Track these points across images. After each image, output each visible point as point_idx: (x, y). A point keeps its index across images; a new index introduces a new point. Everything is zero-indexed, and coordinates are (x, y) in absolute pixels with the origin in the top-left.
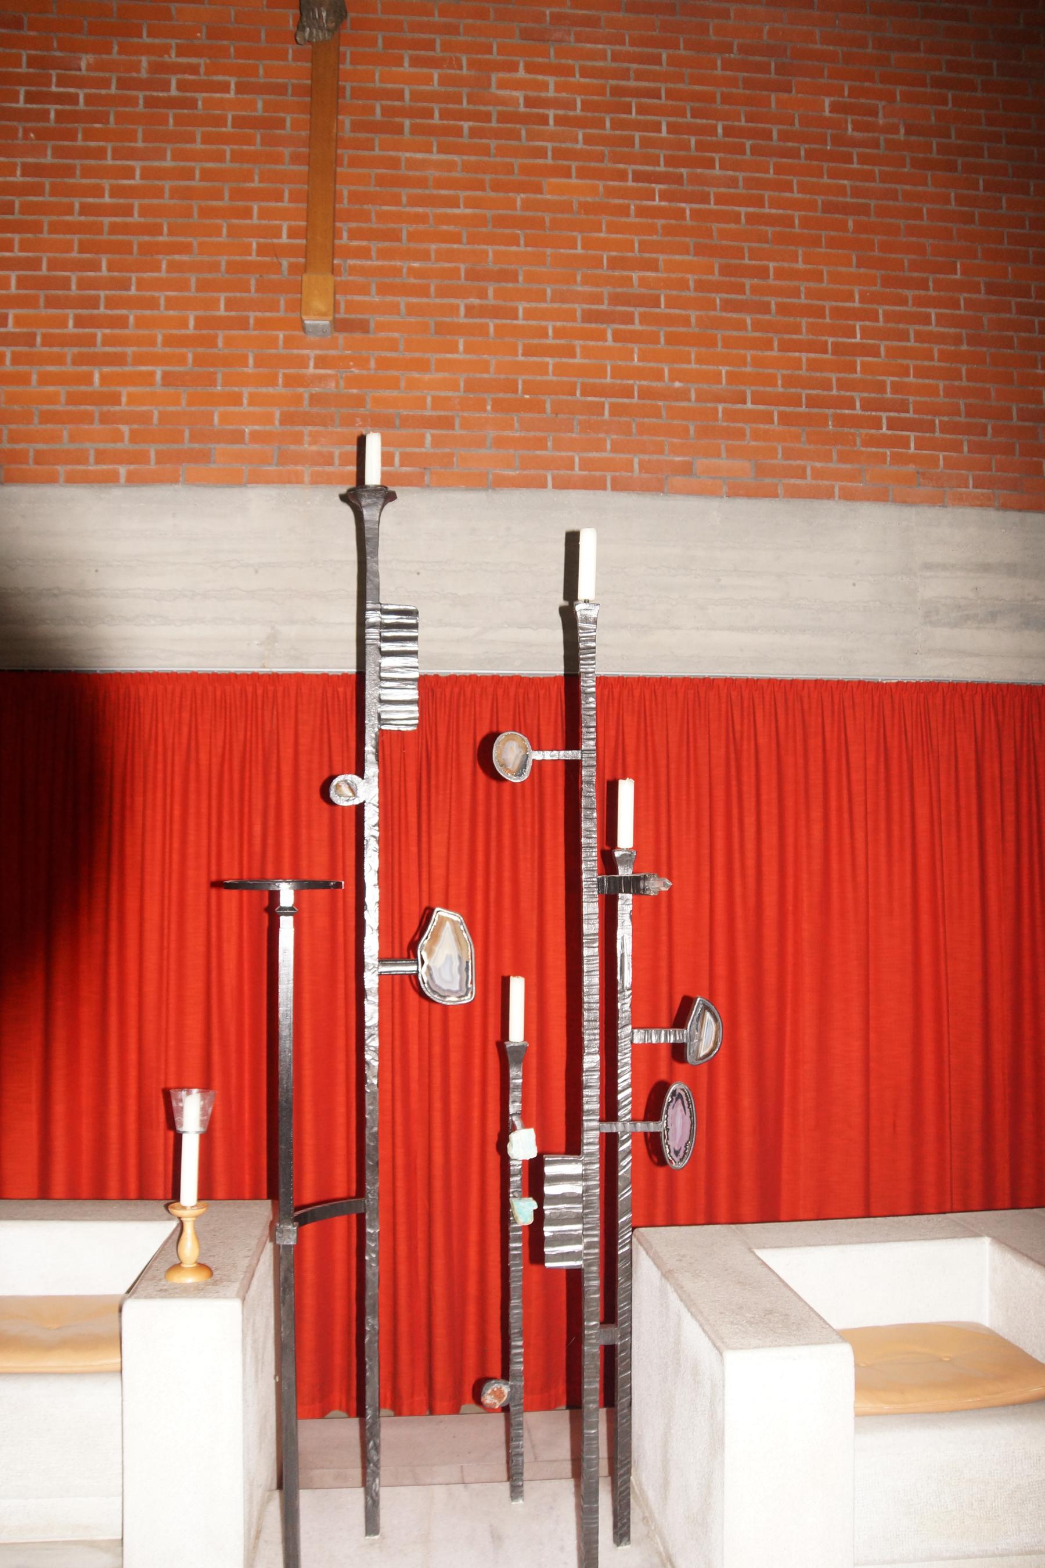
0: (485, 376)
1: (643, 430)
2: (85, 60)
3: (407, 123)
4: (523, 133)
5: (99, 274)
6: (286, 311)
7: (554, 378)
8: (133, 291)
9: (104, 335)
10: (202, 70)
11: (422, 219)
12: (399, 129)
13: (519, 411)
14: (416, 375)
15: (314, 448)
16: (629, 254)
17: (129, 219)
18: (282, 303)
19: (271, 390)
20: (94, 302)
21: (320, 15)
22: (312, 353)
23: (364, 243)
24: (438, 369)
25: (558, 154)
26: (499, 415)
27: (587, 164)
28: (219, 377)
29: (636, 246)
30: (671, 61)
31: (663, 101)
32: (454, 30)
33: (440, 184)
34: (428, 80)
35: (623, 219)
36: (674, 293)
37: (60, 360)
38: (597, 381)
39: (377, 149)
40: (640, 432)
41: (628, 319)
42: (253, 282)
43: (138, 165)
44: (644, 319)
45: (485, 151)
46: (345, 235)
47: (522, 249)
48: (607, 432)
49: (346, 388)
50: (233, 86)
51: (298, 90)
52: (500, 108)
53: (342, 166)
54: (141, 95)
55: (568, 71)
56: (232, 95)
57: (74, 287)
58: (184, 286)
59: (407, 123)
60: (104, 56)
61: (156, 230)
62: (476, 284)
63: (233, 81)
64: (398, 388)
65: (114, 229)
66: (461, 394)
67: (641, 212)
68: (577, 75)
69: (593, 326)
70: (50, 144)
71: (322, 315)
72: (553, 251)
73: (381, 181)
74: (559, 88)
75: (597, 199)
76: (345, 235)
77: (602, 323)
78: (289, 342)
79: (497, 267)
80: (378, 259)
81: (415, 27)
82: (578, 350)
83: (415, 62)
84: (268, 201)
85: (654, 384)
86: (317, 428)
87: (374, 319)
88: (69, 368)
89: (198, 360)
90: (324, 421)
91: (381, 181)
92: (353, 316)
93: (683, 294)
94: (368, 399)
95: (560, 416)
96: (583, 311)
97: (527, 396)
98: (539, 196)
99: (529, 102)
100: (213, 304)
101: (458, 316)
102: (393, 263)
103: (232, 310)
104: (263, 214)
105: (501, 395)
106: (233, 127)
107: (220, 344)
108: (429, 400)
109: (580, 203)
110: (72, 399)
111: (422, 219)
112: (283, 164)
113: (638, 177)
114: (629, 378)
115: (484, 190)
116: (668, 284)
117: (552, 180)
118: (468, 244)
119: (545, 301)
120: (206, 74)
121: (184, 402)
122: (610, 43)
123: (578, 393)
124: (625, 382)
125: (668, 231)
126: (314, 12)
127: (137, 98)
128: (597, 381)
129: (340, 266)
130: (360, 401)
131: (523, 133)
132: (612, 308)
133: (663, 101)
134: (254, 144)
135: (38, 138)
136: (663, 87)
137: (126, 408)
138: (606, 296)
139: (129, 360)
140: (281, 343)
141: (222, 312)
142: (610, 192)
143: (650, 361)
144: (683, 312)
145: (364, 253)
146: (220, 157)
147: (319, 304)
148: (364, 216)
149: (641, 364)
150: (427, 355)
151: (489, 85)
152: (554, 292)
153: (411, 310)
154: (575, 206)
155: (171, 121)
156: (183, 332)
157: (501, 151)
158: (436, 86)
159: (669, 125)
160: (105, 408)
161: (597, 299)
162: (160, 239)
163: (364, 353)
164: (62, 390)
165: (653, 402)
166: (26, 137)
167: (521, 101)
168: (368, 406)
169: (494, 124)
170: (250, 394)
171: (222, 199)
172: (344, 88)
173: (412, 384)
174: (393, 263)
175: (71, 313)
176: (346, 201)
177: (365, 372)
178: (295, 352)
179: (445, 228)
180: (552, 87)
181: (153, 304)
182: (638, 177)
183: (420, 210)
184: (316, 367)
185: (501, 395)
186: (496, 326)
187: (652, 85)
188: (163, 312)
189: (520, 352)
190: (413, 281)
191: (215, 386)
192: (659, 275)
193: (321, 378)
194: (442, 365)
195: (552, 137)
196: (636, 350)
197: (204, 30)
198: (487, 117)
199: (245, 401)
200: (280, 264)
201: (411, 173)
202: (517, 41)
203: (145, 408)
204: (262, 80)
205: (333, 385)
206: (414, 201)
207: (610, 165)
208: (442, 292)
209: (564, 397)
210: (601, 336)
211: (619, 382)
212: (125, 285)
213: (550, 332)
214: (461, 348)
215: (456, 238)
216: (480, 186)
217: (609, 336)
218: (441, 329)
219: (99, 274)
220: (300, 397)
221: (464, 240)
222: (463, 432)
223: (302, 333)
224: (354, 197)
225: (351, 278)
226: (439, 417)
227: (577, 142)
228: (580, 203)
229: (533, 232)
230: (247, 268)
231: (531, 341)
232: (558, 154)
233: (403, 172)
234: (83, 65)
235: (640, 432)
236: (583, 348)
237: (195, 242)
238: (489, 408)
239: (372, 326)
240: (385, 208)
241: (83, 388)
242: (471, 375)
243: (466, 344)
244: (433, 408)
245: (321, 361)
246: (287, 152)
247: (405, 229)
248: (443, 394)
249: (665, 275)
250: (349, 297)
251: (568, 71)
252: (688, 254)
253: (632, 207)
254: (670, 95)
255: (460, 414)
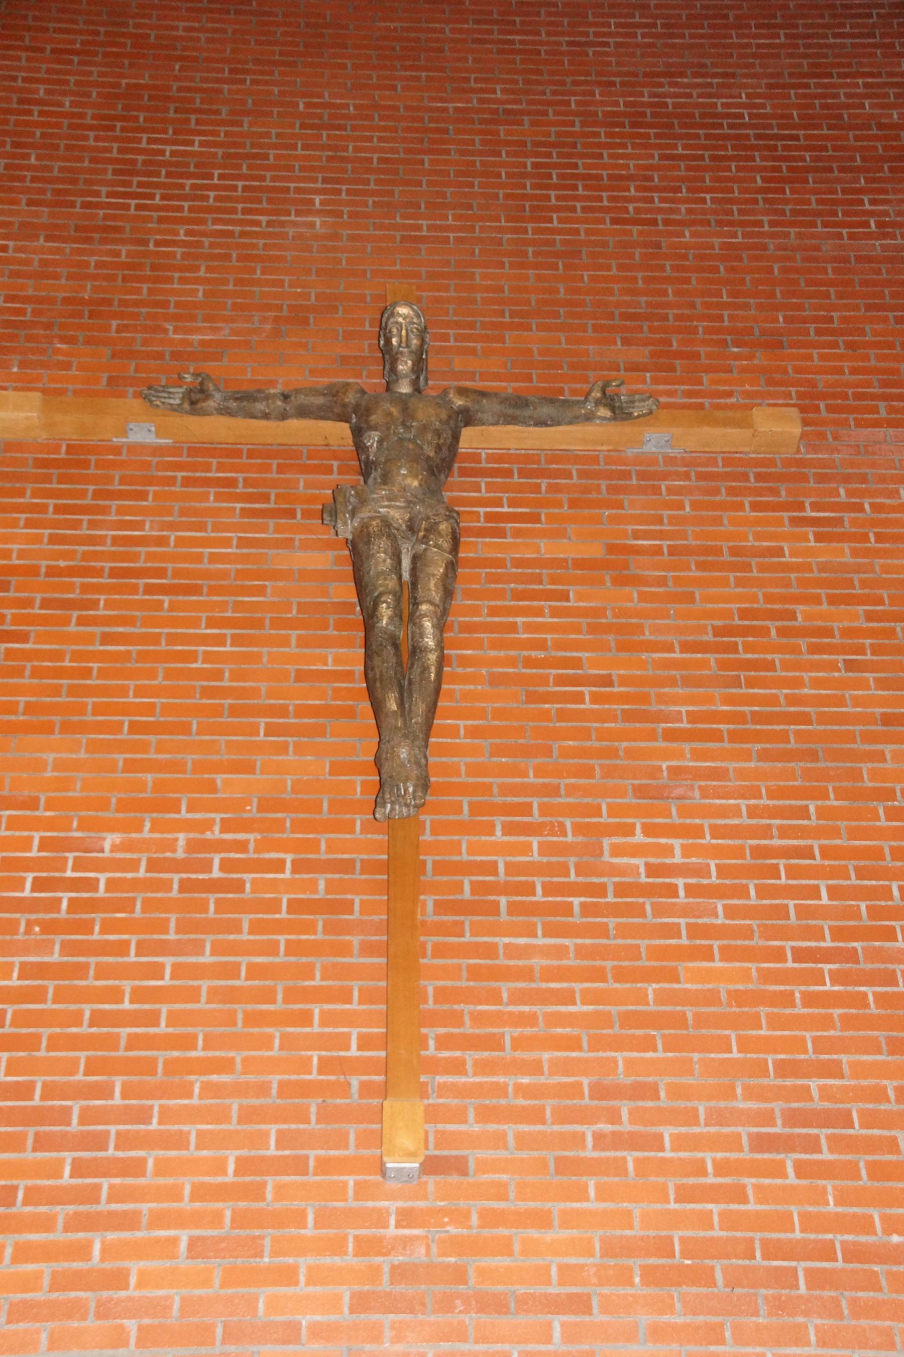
0: (628, 1233)
1: (859, 1309)
2: (110, 839)
3: (503, 901)
4: (648, 908)
5: (110, 1102)
6: (357, 1147)
7: (723, 1234)
8: (154, 1125)
9: (111, 1187)
10: (251, 847)
11: (530, 1020)
12: (494, 909)
13: (679, 1285)
14: (533, 1233)
15: (399, 1348)
16: (802, 1057)
17: (153, 1030)
18: (352, 1137)
19: (337, 1260)
20: (100, 1141)
21: (406, 790)
22: (392, 1206)
23: (458, 1054)
24: (565, 1225)
25: (694, 931)
26: (651, 1290)
27: (733, 943)
28: (267, 1243)
29: (810, 1045)
30: (822, 813)
31: (818, 861)
32: (554, 791)
33: (550, 974)
34: (526, 849)
35: (788, 1011)
36: (870, 1106)
37: (47, 1223)
38: (782, 1236)
39: (468, 934)
40: (856, 1315)
41: (813, 1145)
42: (313, 1110)
43: (168, 962)
44: (836, 1144)
45: (603, 931)
46: (432, 1043)
47: (660, 1054)
48: (807, 1314)
49: (440, 1256)
50: (288, 865)
51: (368, 867)
52: (617, 879)
53: (424, 956)
54: (176, 877)
55: (697, 832)
56: (287, 875)
57: (75, 1120)
58: (222, 1115)
59: (503, 901)
60: (134, 835)
61: (188, 1043)
62: (604, 1103)
63: (289, 858)
64: (510, 1254)
65: (134, 1042)
66: (597, 1260)
67: (810, 1000)
68: (708, 837)
69: (766, 1156)
70: (59, 939)
71: (412, 1155)
72: (701, 1055)
73: (475, 973)
74: (687, 851)
75: (751, 987)
76: (432, 1043)
77: (778, 1151)
78: (362, 1191)
79: (629, 1080)
80: (475, 1074)
81: (505, 790)
82: (750, 1192)
83: (509, 829)
84: (334, 1002)
85: (863, 1239)
86: (400, 1317)
87: (474, 1156)
88: (58, 1236)
89: (239, 1220)
90: (411, 1306)
91: (475, 973)
92: (446, 1153)
93: (883, 1107)
94: (471, 1272)
95: (738, 1290)
96: (750, 1135)
97: (688, 1262)
98: (676, 986)
99: (652, 870)
100: (261, 1139)
101: (584, 1148)
102: (495, 1079)
103: (284, 1149)
104: (328, 1019)
105: (652, 1261)
106: (288, 912)
107: (269, 1196)
108: (554, 1271)
109: (729, 992)
110: (60, 1282)
111: (530, 1020)
112: (352, 956)
113: (800, 955)
114: (826, 1231)
115: (605, 980)
116: (860, 1095)
117: (690, 964)
118: (590, 1051)
119: (697, 1124)
120: (255, 851)
121: (217, 1282)
122: (744, 797)
123: (758, 1254)
124: (821, 1236)
125: (848, 1022)
126: (398, 789)
127: (171, 881)
128: (782, 1236)
129: (427, 1084)
130: (460, 1276)
131: (648, 908)
132: (788, 1130)
133: (818, 861)
134: (315, 933)
135: (43, 932)
136: (816, 844)
137: (137, 1293)
138: (778, 1114)
139: (144, 1221)
140: (351, 1192)
141: (272, 1151)
142: (766, 976)
143: (852, 1205)
144: (886, 1133)
145: (458, 1067)
146: (272, 949)
147: (406, 1140)
148: (456, 1019)
149: (839, 1209)
150: (548, 1205)
151: (601, 854)
152: (709, 1111)
153: (523, 1141)
154: (723, 996)
155: (212, 907)
156: (220, 1179)
157: (624, 931)
158: (536, 856)
159: (829, 889)
160: (105, 1294)
161: (767, 1118)
162: (193, 1054)
163: (463, 1204)
164: (46, 1269)
165: (866, 1266)
166: (28, 931)
167: (642, 870)
168: (471, 1282)
169: (610, 899)
170: (310, 1268)
171: (273, 1001)
172: (424, 863)
173: (530, 1248)
174: (495, 1079)
175: (68, 1157)
176: (431, 1001)
177: (465, 1231)
178: (370, 1204)
179: (559, 1030)
180: (678, 851)
181: (180, 1141)
182: (800, 955)
183: (526, 1009)
184: (398, 1225)
185: (652, 1261)
186: (637, 1161)
187: (801, 842)
188: (192, 1152)
189: (672, 1197)
190: (521, 1102)
191: (262, 1257)
192: (845, 1082)
193: (406, 1242)
194: (568, 1219)
195: (685, 911)
196: (830, 1189)
197: (255, 802)
198: (601, 890)
199: (302, 1279)
200: (349, 1084)
201: (512, 963)
202: (630, 800)
203: (161, 1293)
204: (324, 857)
205: (423, 1250)
206: (518, 997)
207: (762, 943)
208: (562, 1116)
209: (740, 1262)
210: (779, 1170)
211: (812, 1236)
212: (144, 1116)
213: (710, 1168)
214: (592, 1193)
215: (573, 1044)
216: (599, 975)
217: (790, 1170)
218: (564, 1166)
219: (110, 1102)
220: (378, 1269)
221: (585, 1045)
222: (605, 1318)
223: (379, 1178)
224: (442, 995)
225: (441, 1101)
226: (570, 1296)
227: (716, 916)
228: (729, 992)
229: (672, 1032)
230: (306, 1089)
231: (685, 1181)
232: (694, 931)
233: (502, 961)
234: (107, 846)
235: (856, 1315)
236: (758, 1188)
237: (238, 1056)
238: (637, 1280)
239: (472, 1165)
240: (480, 1008)
241: (77, 1265)
242: (610, 1232)
243: (598, 1187)
244: (561, 1283)
245: (406, 1218)
246: (356, 940)
247: (509, 1033)
248: (572, 1260)
249: (853, 1082)
250: (440, 1126)
251: (697, 832)
252: (880, 1053)
253: (797, 995)
254: (826, 853)
255: (599, 1290)
